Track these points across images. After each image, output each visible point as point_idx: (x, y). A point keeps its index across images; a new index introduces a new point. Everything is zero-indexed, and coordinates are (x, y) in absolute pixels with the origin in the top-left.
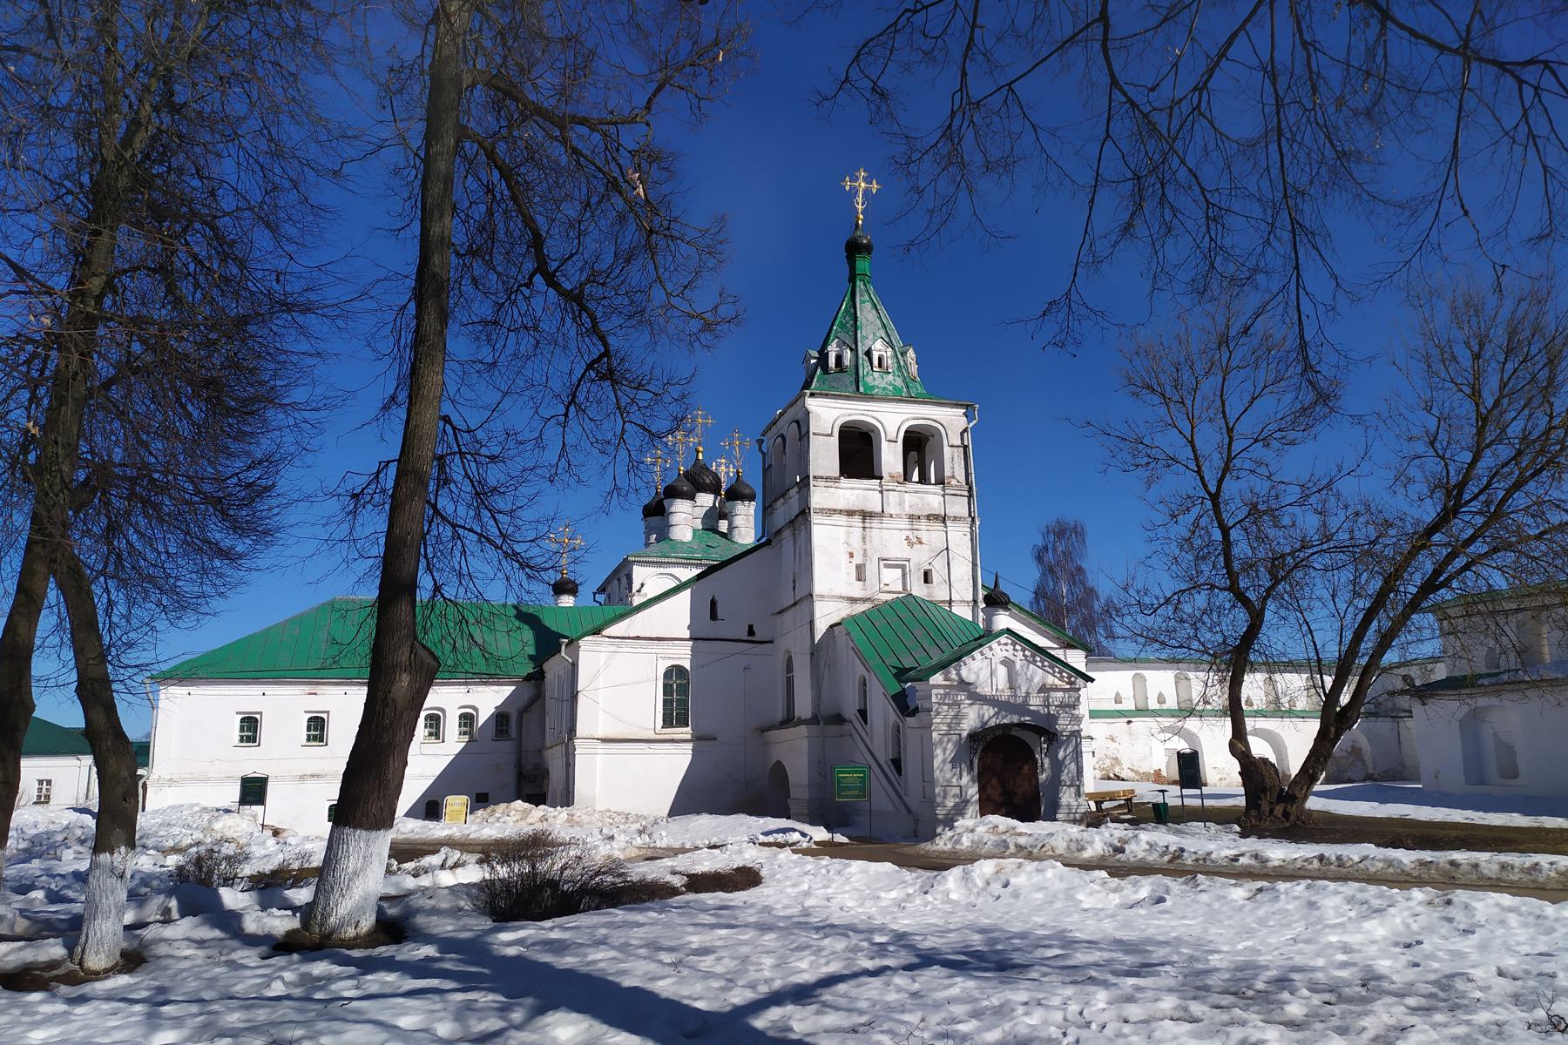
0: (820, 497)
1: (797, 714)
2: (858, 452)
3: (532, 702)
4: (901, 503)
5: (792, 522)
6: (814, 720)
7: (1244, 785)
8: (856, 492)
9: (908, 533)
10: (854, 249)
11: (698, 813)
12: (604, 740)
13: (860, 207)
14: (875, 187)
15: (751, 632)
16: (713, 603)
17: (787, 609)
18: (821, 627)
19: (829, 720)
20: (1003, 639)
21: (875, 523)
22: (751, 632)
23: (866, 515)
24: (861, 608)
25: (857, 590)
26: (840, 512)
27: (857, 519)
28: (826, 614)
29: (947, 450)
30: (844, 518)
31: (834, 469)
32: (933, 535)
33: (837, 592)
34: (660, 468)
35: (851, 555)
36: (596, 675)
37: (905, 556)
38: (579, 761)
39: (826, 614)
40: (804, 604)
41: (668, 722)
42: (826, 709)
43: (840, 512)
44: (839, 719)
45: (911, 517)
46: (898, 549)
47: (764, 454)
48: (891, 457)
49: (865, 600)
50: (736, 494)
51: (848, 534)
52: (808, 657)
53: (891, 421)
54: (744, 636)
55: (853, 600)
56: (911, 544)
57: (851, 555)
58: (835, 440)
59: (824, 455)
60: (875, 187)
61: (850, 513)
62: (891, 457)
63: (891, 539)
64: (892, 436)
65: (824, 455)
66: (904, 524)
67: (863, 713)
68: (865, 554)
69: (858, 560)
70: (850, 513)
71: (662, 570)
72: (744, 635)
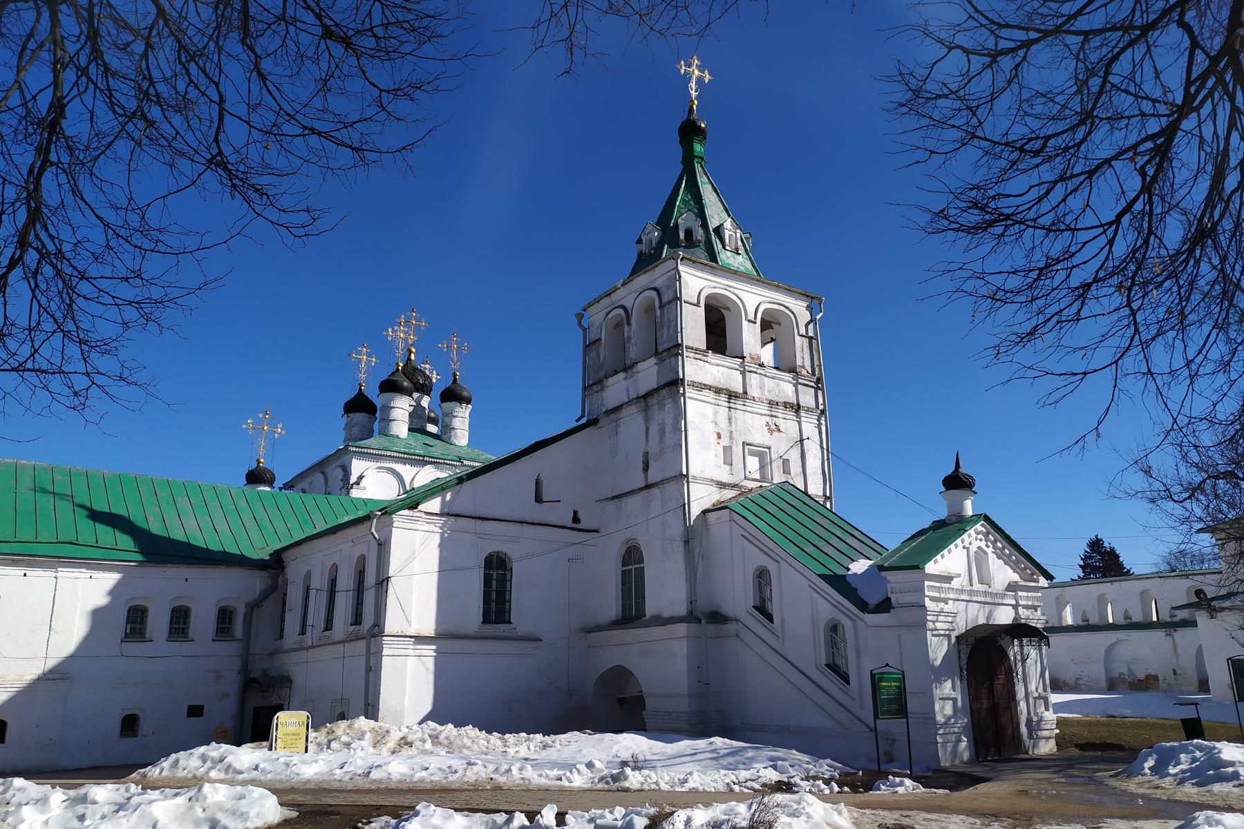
1: (650, 609)
3: (266, 594)
4: (762, 387)
5: (645, 396)
6: (691, 617)
9: (768, 419)
10: (690, 131)
11: (617, 731)
13: (694, 94)
14: (707, 78)
15: (576, 519)
16: (538, 483)
17: (631, 493)
18: (695, 511)
19: (707, 617)
20: (979, 527)
21: (739, 404)
22: (576, 519)
23: (731, 395)
24: (729, 494)
25: (726, 478)
26: (710, 388)
27: (724, 398)
28: (700, 498)
29: (797, 338)
30: (712, 394)
31: (702, 345)
33: (708, 475)
34: (366, 369)
35: (719, 436)
36: (412, 558)
37: (767, 443)
38: (386, 662)
39: (700, 498)
40: (671, 488)
41: (487, 619)
42: (703, 606)
43: (710, 388)
44: (717, 617)
46: (759, 436)
47: (585, 330)
48: (750, 336)
49: (734, 486)
50: (452, 395)
51: (716, 412)
52: (679, 547)
54: (570, 523)
55: (722, 485)
56: (771, 431)
58: (701, 311)
59: (693, 328)
60: (707, 78)
61: (718, 391)
65: (693, 328)
66: (764, 409)
67: (763, 610)
68: (731, 437)
70: (718, 391)
71: (379, 464)
72: (568, 522)
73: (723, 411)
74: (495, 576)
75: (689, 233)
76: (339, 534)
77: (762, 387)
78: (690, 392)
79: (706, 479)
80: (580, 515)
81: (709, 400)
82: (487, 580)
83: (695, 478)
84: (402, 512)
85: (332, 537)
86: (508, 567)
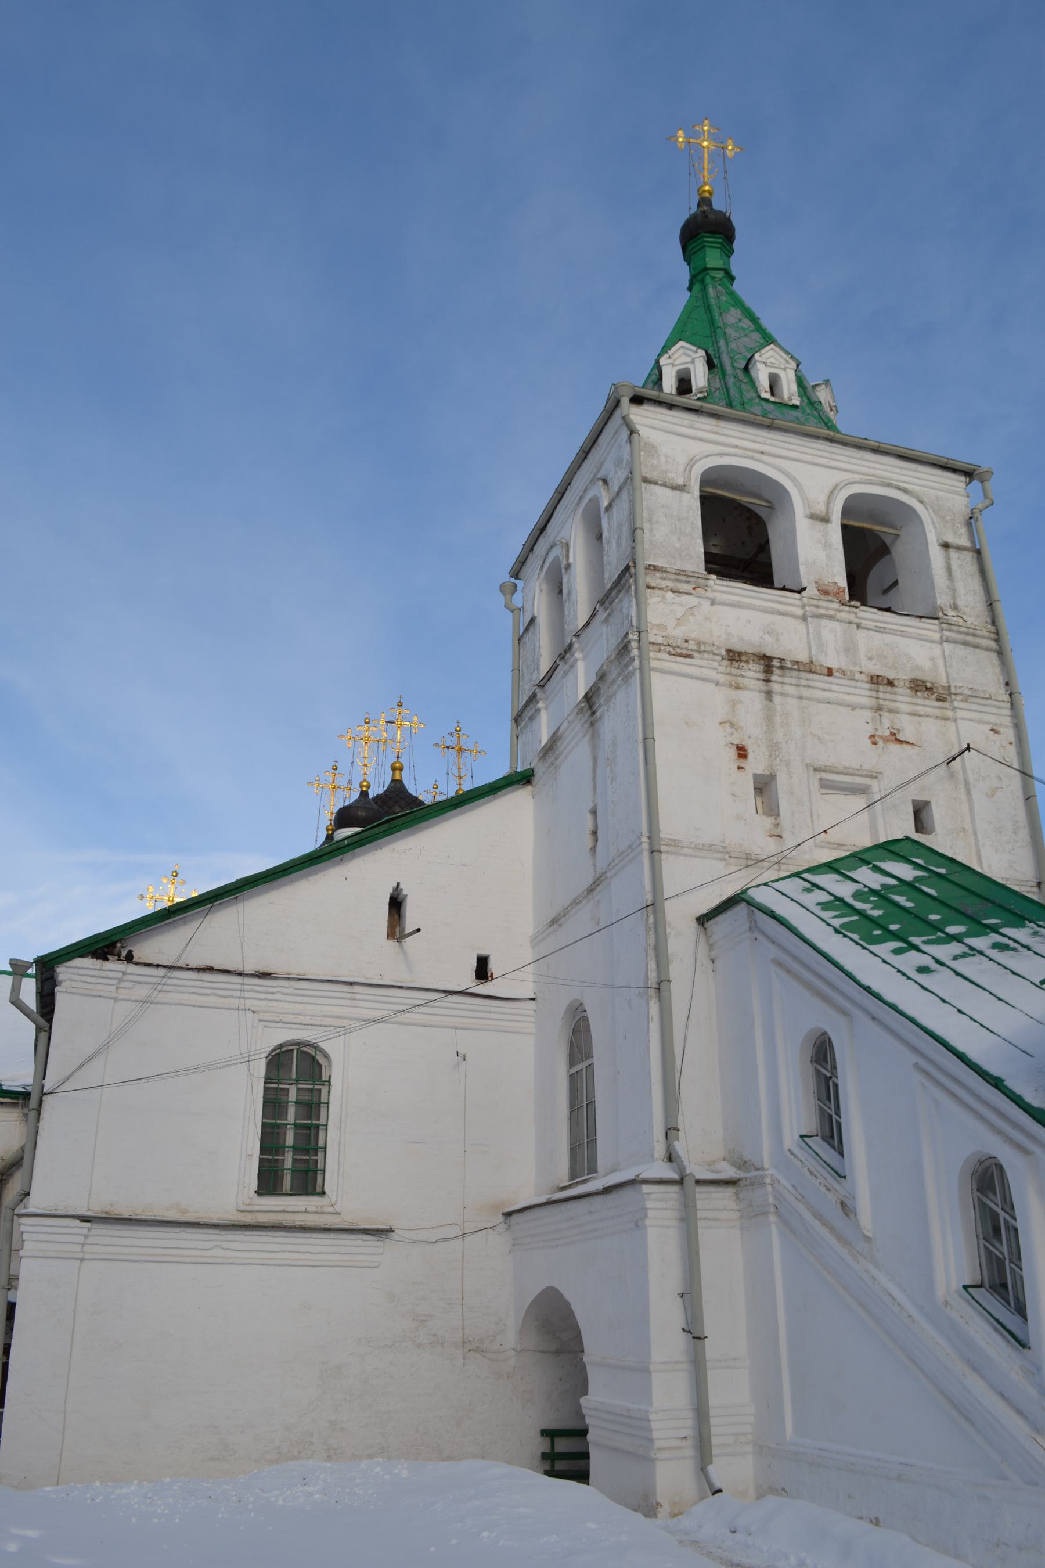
0: (665, 612)
2: (740, 539)
4: (850, 649)
7: (11, 1250)
8: (739, 613)
12: (85, 1219)
15: (482, 969)
16: (396, 904)
22: (482, 969)
27: (752, 672)
31: (696, 562)
32: (929, 730)
35: (742, 752)
41: (269, 1181)
45: (875, 680)
48: (815, 551)
51: (734, 704)
53: (813, 486)
55: (751, 861)
57: (742, 752)
58: (691, 505)
59: (675, 530)
62: (815, 551)
63: (834, 727)
64: (820, 508)
66: (862, 694)
68: (774, 748)
69: (757, 763)
73: (752, 699)
74: (292, 1095)
75: (684, 385)
76: (525, 1213)
77: (850, 649)
78: (658, 660)
79: (709, 848)
80: (493, 966)
81: (713, 674)
82: (273, 1104)
83: (675, 843)
84: (79, 962)
85: (520, 1215)
86: (325, 1077)
